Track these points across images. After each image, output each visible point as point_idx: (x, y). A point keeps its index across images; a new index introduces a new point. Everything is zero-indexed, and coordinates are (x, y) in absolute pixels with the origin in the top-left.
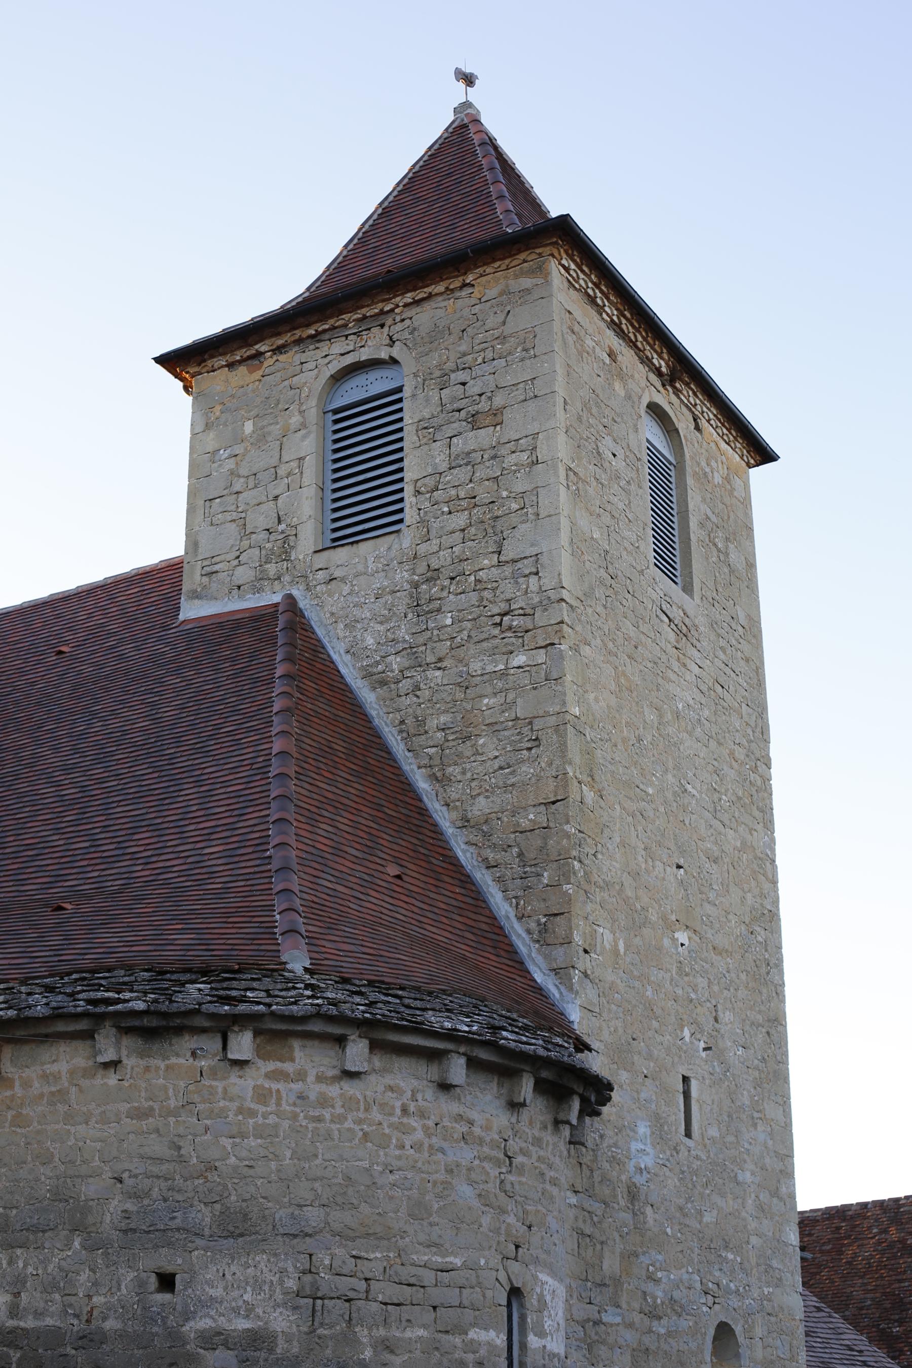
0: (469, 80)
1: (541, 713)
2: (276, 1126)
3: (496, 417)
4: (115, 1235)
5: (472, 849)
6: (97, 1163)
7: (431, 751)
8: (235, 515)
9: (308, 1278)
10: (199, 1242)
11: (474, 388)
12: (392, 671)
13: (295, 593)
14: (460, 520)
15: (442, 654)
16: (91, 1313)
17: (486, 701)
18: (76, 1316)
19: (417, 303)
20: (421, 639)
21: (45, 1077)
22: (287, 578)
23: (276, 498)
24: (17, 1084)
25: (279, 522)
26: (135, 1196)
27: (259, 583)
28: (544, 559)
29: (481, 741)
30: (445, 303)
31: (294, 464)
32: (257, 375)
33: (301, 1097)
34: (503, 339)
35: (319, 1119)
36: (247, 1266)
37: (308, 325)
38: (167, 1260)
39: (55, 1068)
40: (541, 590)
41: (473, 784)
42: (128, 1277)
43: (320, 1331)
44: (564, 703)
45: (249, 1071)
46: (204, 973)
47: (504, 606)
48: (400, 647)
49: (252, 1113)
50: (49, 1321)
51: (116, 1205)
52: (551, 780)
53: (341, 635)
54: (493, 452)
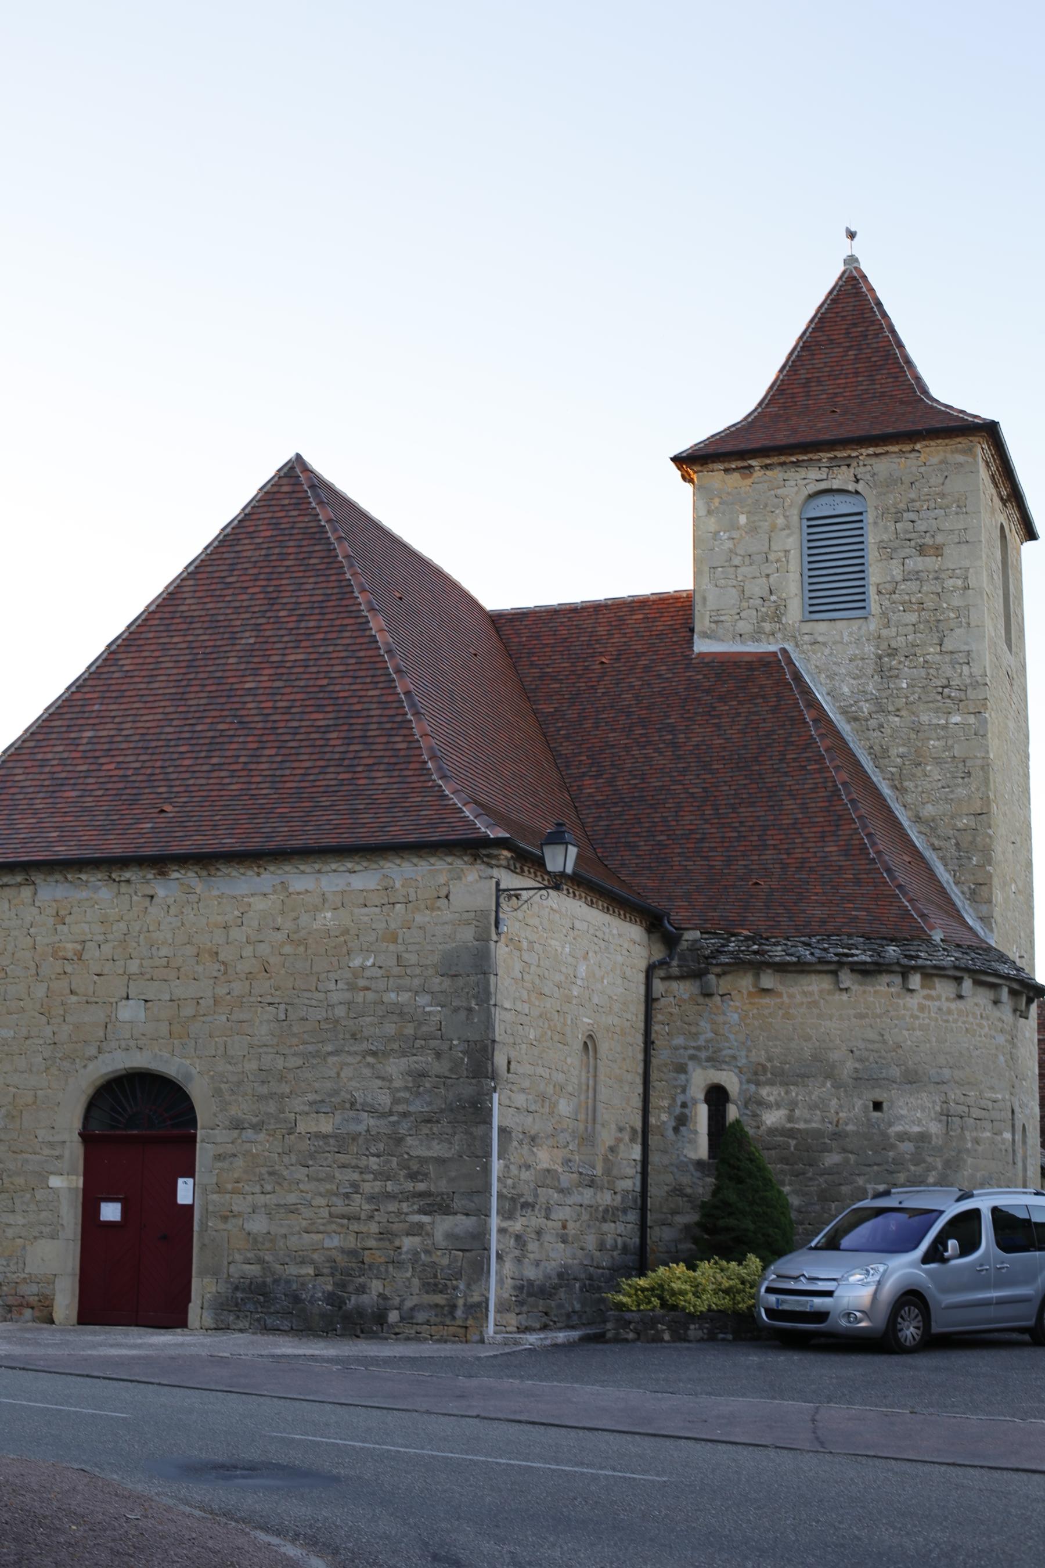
0: (852, 235)
1: (971, 756)
2: (929, 1025)
3: (938, 551)
4: (850, 1081)
5: (923, 837)
6: (838, 1042)
7: (893, 770)
8: (735, 583)
9: (945, 1106)
10: (895, 1086)
11: (921, 526)
12: (863, 712)
13: (787, 647)
14: (913, 618)
15: (899, 707)
16: (838, 1122)
17: (932, 742)
18: (830, 1123)
19: (876, 455)
20: (884, 695)
21: (804, 993)
22: (779, 635)
23: (768, 576)
24: (785, 996)
25: (771, 593)
26: (861, 1060)
27: (757, 635)
28: (974, 655)
29: (928, 768)
30: (899, 460)
31: (782, 554)
32: (749, 481)
33: (940, 1009)
34: (943, 496)
35: (947, 1021)
36: (918, 1098)
37: (792, 455)
38: (879, 1095)
39: (810, 988)
40: (971, 675)
41: (924, 795)
42: (859, 1103)
43: (951, 1133)
44: (988, 752)
45: (915, 995)
46: (892, 940)
47: (945, 682)
48: (869, 697)
49: (917, 1017)
50: (814, 1125)
51: (850, 1065)
52: (978, 800)
53: (823, 681)
54: (936, 575)
